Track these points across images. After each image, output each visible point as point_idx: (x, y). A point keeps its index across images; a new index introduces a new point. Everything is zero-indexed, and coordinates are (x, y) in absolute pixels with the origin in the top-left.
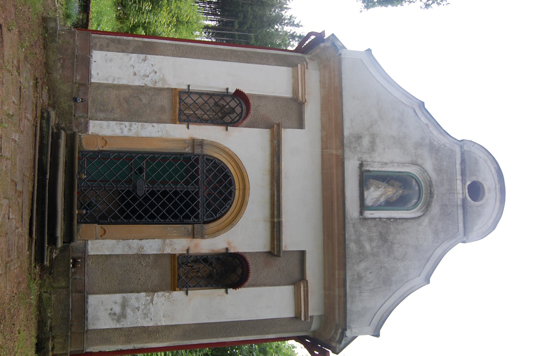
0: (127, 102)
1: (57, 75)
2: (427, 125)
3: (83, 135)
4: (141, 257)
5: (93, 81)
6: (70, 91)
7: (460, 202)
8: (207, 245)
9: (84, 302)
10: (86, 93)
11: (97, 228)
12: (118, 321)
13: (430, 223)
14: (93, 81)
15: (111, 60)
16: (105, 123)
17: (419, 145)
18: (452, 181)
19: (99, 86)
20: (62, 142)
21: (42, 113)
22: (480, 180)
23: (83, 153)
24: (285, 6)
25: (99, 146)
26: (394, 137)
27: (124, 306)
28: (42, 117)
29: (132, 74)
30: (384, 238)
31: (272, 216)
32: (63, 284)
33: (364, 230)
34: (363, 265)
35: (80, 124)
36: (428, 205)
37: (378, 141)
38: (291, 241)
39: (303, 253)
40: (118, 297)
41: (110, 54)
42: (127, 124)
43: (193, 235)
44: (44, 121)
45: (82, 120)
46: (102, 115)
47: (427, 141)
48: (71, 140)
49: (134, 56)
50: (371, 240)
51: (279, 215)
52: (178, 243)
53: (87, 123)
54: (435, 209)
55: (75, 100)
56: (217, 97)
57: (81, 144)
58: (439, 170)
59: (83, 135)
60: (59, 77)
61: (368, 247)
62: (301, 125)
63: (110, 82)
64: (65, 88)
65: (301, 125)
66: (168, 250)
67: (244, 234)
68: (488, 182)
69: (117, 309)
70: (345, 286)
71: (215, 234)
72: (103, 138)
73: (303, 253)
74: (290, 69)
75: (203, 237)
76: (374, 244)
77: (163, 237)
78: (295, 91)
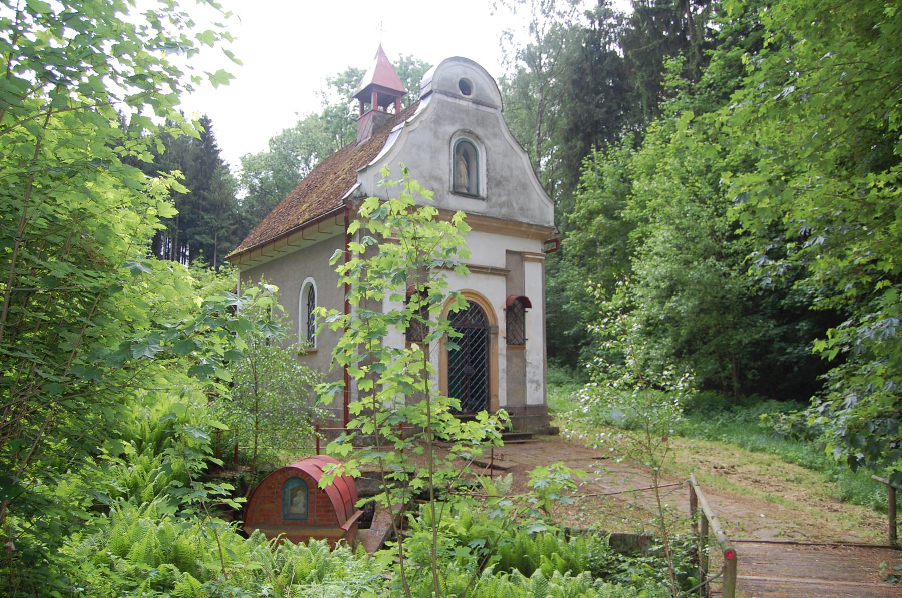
2: (421, 122)
4: (508, 371)
7: (474, 106)
8: (502, 325)
9: (531, 407)
11: (493, 400)
12: (539, 385)
13: (488, 139)
17: (436, 135)
18: (460, 109)
22: (458, 80)
24: (163, 227)
26: (432, 158)
27: (533, 382)
30: (499, 184)
31: (485, 273)
32: (522, 420)
33: (494, 199)
34: (515, 205)
36: (477, 138)
37: (435, 174)
38: (500, 262)
39: (508, 252)
40: (528, 385)
43: (496, 334)
47: (433, 125)
50: (500, 195)
51: (487, 269)
52: (501, 344)
54: (479, 131)
56: (381, 420)
58: (453, 120)
61: (504, 199)
66: (504, 352)
67: (495, 294)
68: (458, 73)
69: (534, 385)
70: (532, 225)
71: (495, 318)
73: (508, 252)
75: (498, 327)
76: (502, 193)
77: (497, 354)
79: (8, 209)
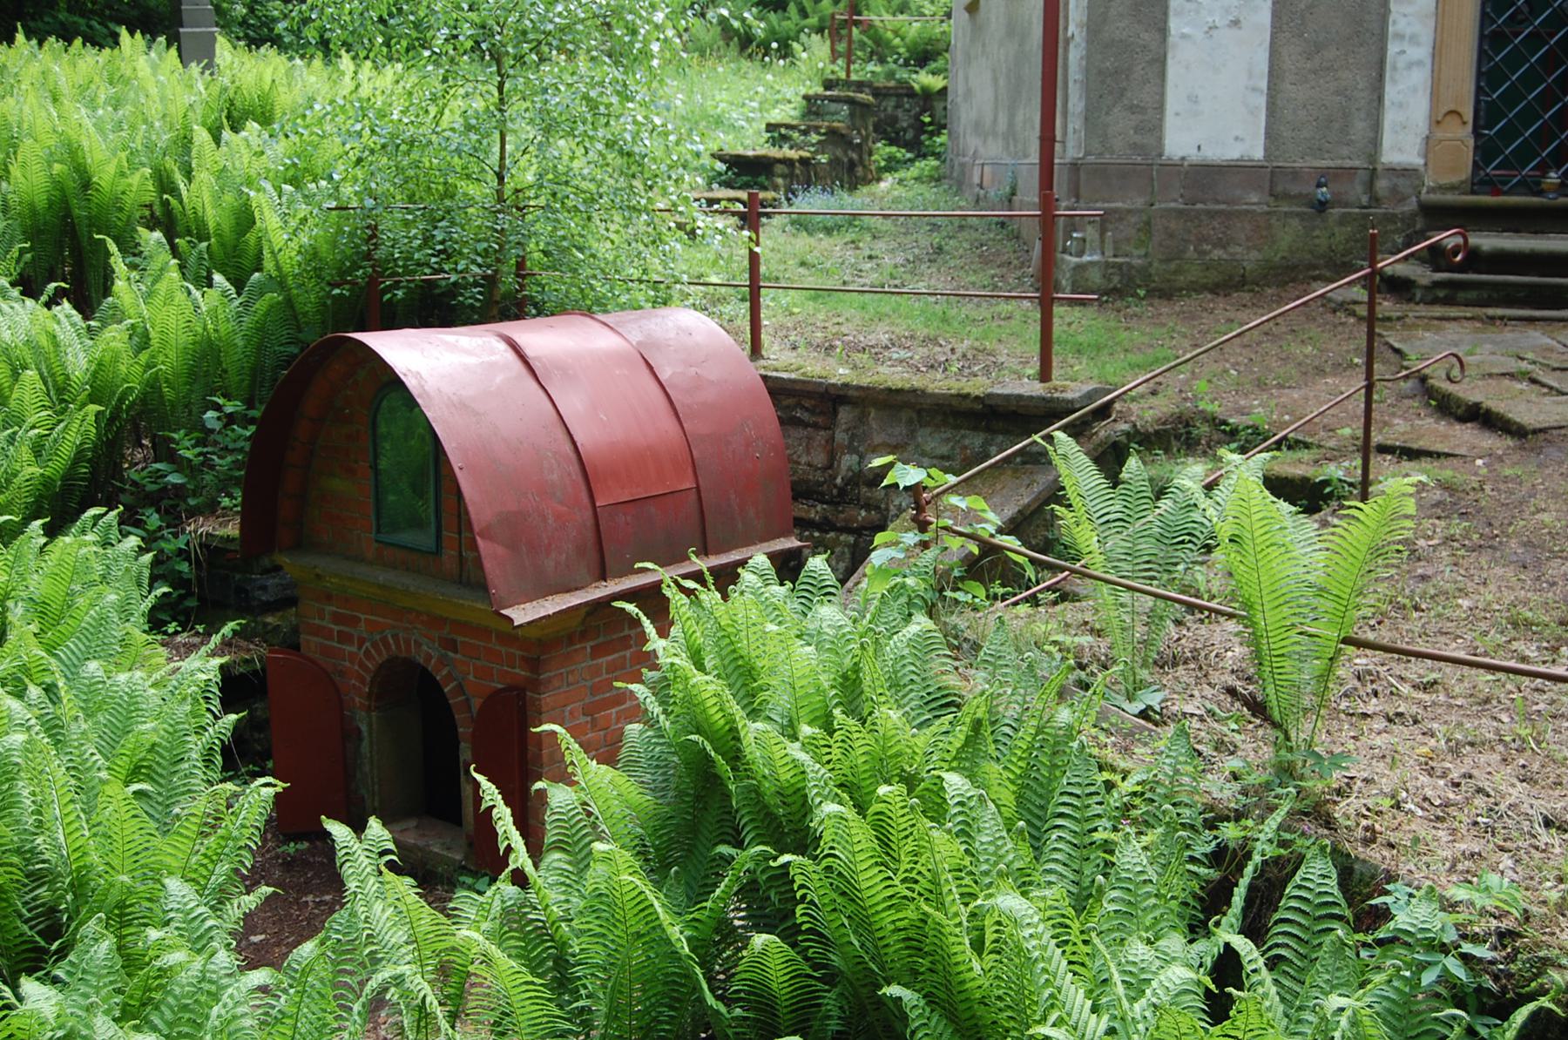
0: (1319, 48)
1: (1250, 259)
3: (1429, 182)
5: (1258, 153)
6: (1295, 222)
10: (1295, 174)
14: (1258, 153)
15: (1193, 99)
16: (1390, 117)
19: (1271, 135)
20: (1487, 241)
21: (1435, 301)
23: (1479, 183)
25: (1462, 136)
28: (1448, 301)
29: (1234, 32)
35: (1394, 190)
41: (1174, 100)
42: (1393, 48)
44: (1461, 295)
45: (1382, 185)
46: (1360, 127)
48: (1437, 215)
49: (1175, 25)
53: (1392, 170)
55: (1322, 206)
57: (1452, 188)
59: (1429, 182)
60: (1254, 255)
63: (1262, 101)
64: (1288, 237)
72: (1435, 122)
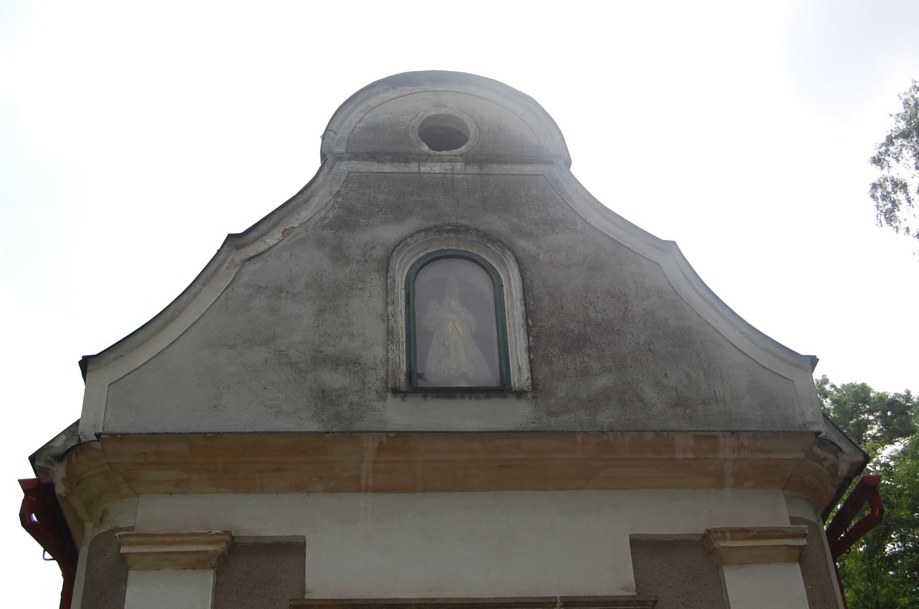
39: (638, 544)
62: (294, 548)
65: (294, 548)
73: (638, 544)
74: (132, 576)
78: (197, 563)
79: (867, 562)
